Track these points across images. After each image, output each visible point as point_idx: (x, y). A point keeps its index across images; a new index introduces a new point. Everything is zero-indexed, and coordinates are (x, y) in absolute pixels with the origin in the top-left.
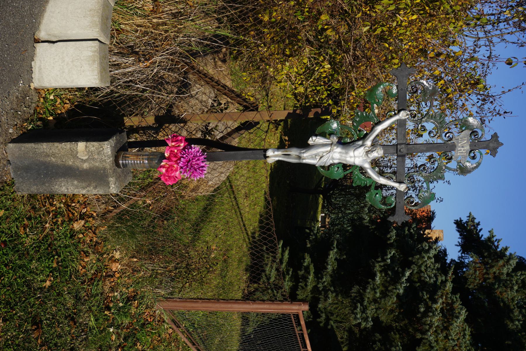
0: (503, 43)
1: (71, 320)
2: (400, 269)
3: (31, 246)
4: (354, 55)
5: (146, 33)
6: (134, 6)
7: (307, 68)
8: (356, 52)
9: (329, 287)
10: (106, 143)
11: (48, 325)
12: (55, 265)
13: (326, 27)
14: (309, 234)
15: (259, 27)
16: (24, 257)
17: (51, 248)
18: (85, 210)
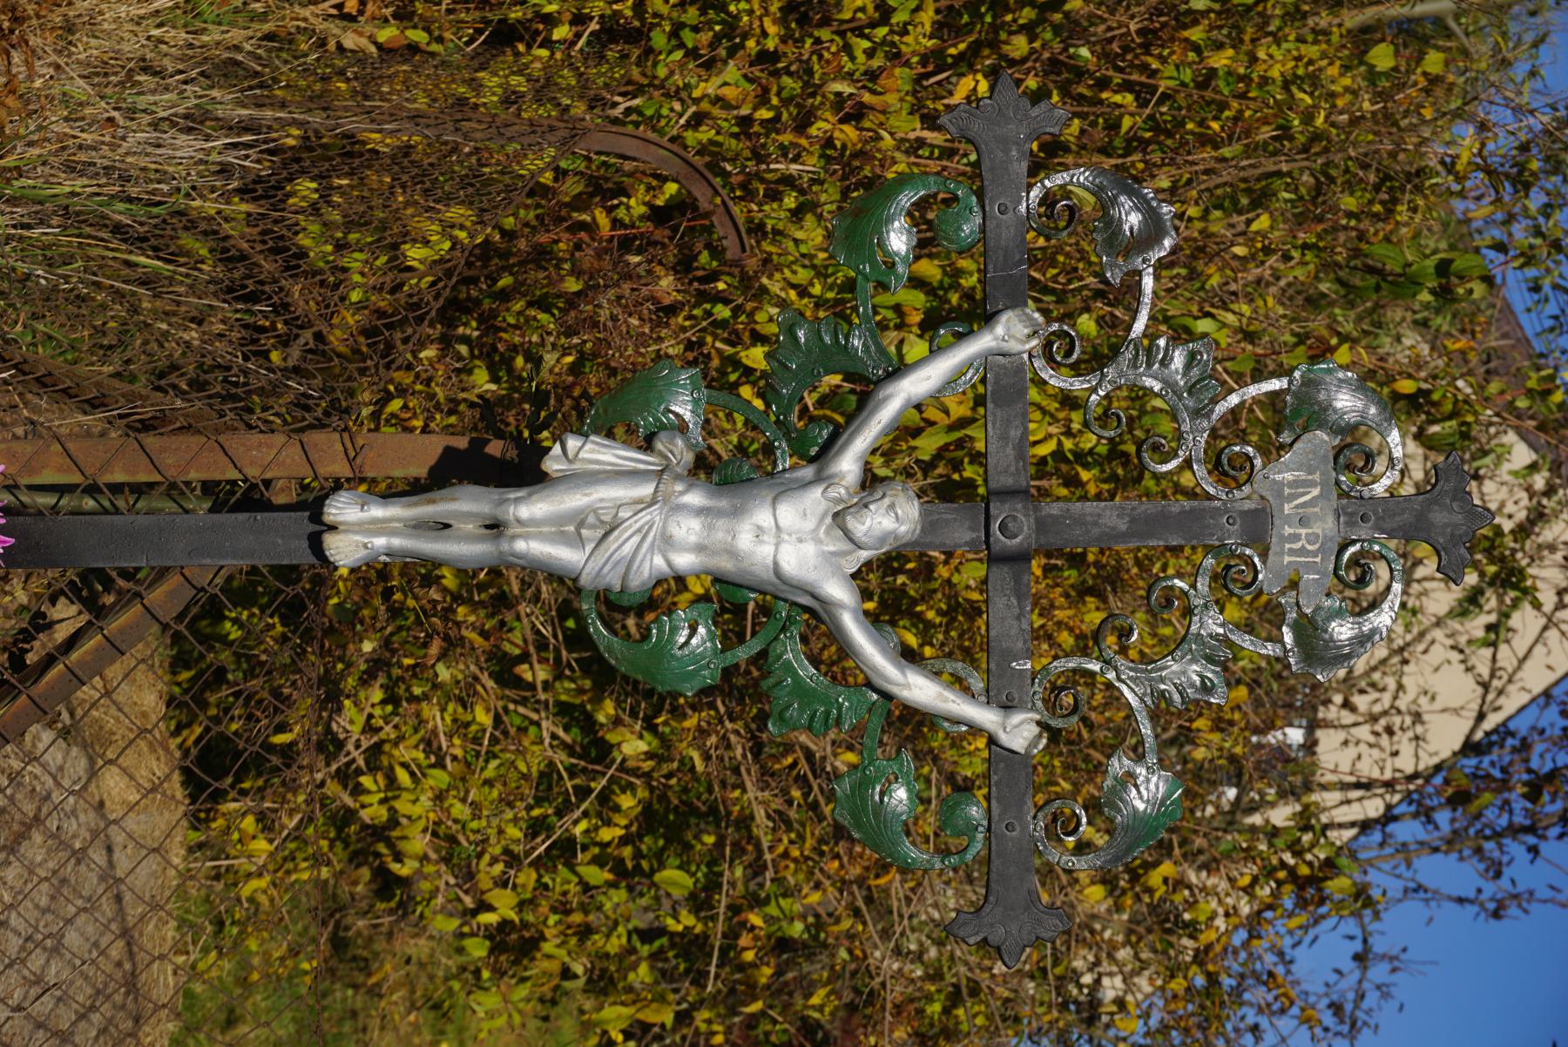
0: (1414, 907)
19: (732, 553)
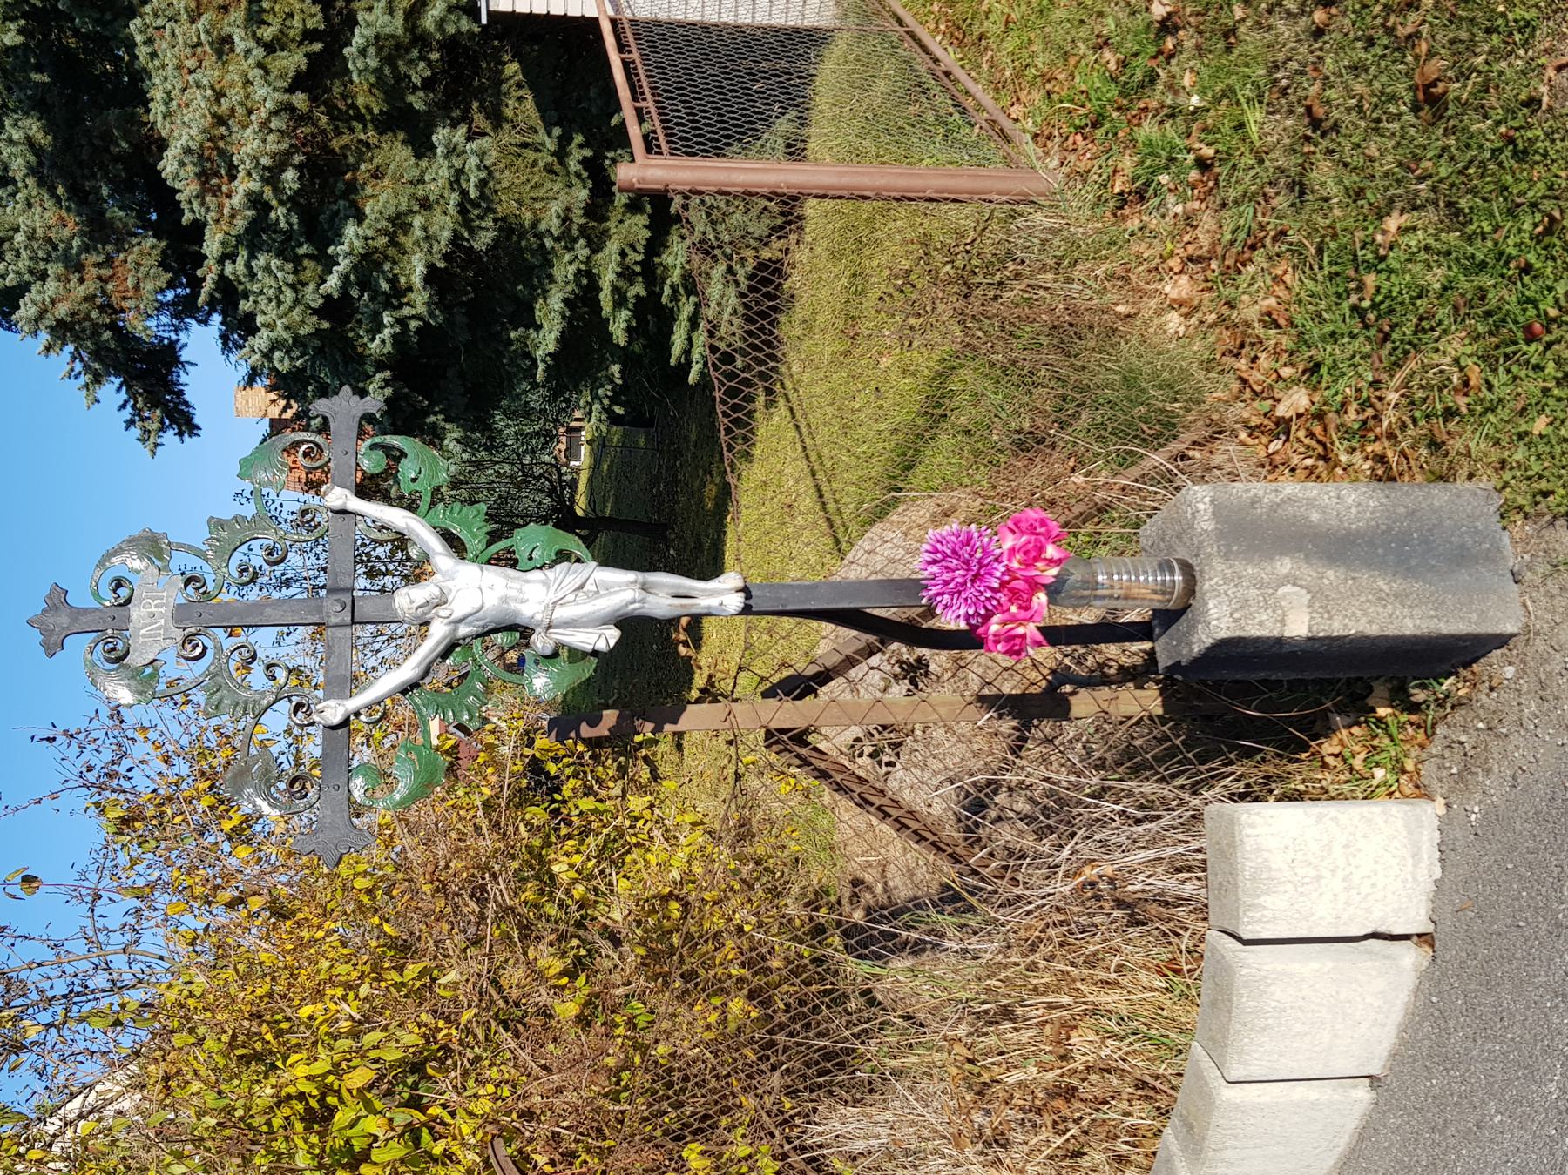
0: (57, 936)
1: (1321, 121)
2: (354, 293)
3: (1445, 332)
4: (483, 902)
5: (1092, 962)
6: (1127, 1041)
7: (618, 864)
8: (477, 910)
9: (557, 246)
10: (1223, 634)
11: (1393, 98)
12: (1371, 280)
13: (565, 980)
14: (614, 400)
15: (759, 981)
16: (1469, 296)
17: (1380, 331)
18: (1272, 448)
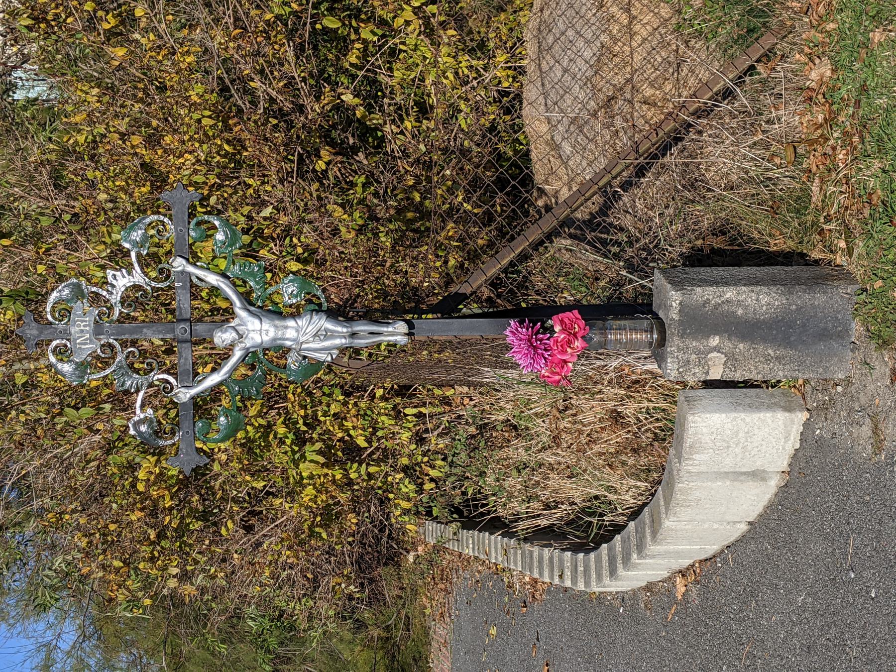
19: (276, 327)
